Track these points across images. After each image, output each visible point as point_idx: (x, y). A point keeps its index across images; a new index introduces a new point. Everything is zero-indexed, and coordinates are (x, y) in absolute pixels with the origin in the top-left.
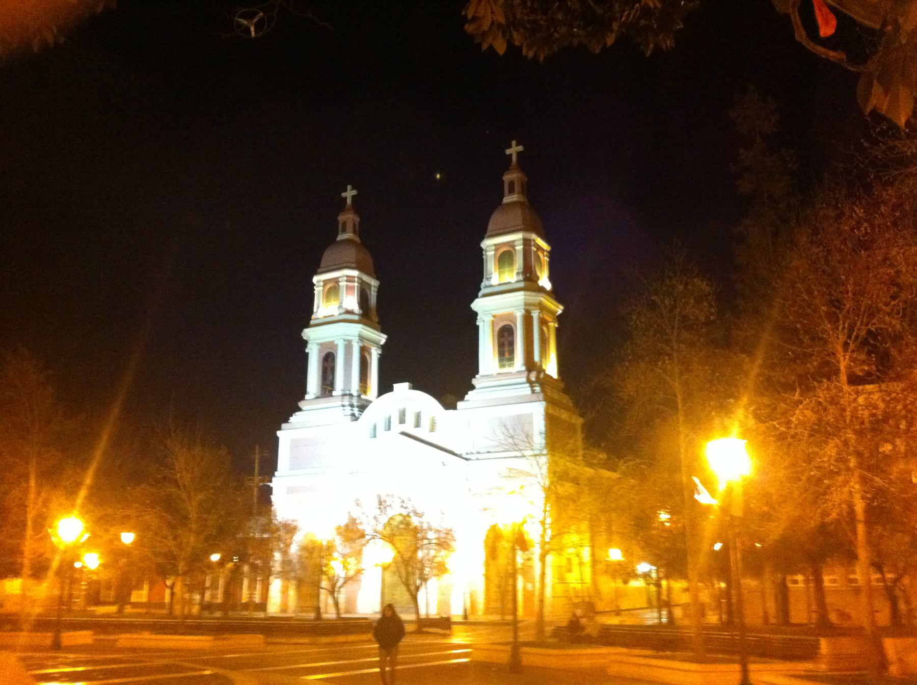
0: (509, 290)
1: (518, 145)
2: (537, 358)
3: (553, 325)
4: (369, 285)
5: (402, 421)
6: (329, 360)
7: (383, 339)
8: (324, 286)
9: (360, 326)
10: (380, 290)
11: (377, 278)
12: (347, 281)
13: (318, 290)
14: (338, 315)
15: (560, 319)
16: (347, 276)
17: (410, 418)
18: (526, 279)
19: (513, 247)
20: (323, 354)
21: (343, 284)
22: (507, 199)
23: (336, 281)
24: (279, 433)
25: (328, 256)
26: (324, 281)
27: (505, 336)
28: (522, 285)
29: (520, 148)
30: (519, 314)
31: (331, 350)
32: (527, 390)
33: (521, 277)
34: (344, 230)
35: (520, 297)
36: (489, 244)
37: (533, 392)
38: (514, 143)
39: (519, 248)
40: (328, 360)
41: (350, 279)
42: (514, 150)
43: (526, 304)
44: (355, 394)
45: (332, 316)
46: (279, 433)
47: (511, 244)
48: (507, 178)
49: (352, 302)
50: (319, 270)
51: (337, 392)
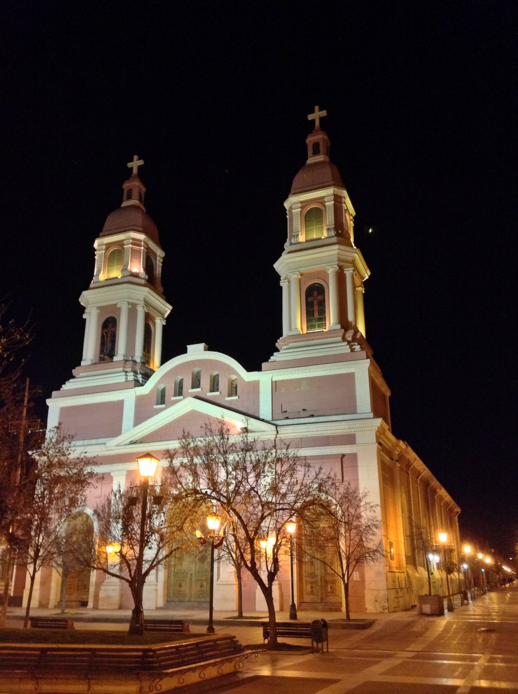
0: (317, 246)
1: (320, 110)
2: (351, 318)
3: (361, 290)
4: (155, 255)
5: (196, 383)
6: (110, 325)
7: (168, 309)
8: (107, 249)
9: (147, 289)
10: (165, 261)
11: (163, 249)
12: (132, 244)
13: (99, 255)
14: (121, 274)
15: (366, 284)
16: (133, 239)
17: (206, 382)
18: (338, 235)
19: (323, 203)
20: (103, 320)
21: (128, 246)
22: (311, 160)
23: (121, 243)
24: (49, 402)
25: (111, 220)
26: (107, 244)
27: (314, 299)
28: (335, 240)
29: (324, 113)
30: (331, 271)
31: (112, 315)
32: (345, 349)
33: (333, 233)
34: (129, 197)
35: (334, 251)
36: (293, 203)
37: (352, 350)
38: (317, 108)
39: (330, 204)
40: (109, 326)
41: (136, 242)
42: (317, 115)
43: (339, 260)
44: (138, 360)
45: (117, 278)
46: (49, 402)
47: (321, 200)
48: (310, 140)
49: (137, 267)
50: (101, 234)
51: (119, 357)
